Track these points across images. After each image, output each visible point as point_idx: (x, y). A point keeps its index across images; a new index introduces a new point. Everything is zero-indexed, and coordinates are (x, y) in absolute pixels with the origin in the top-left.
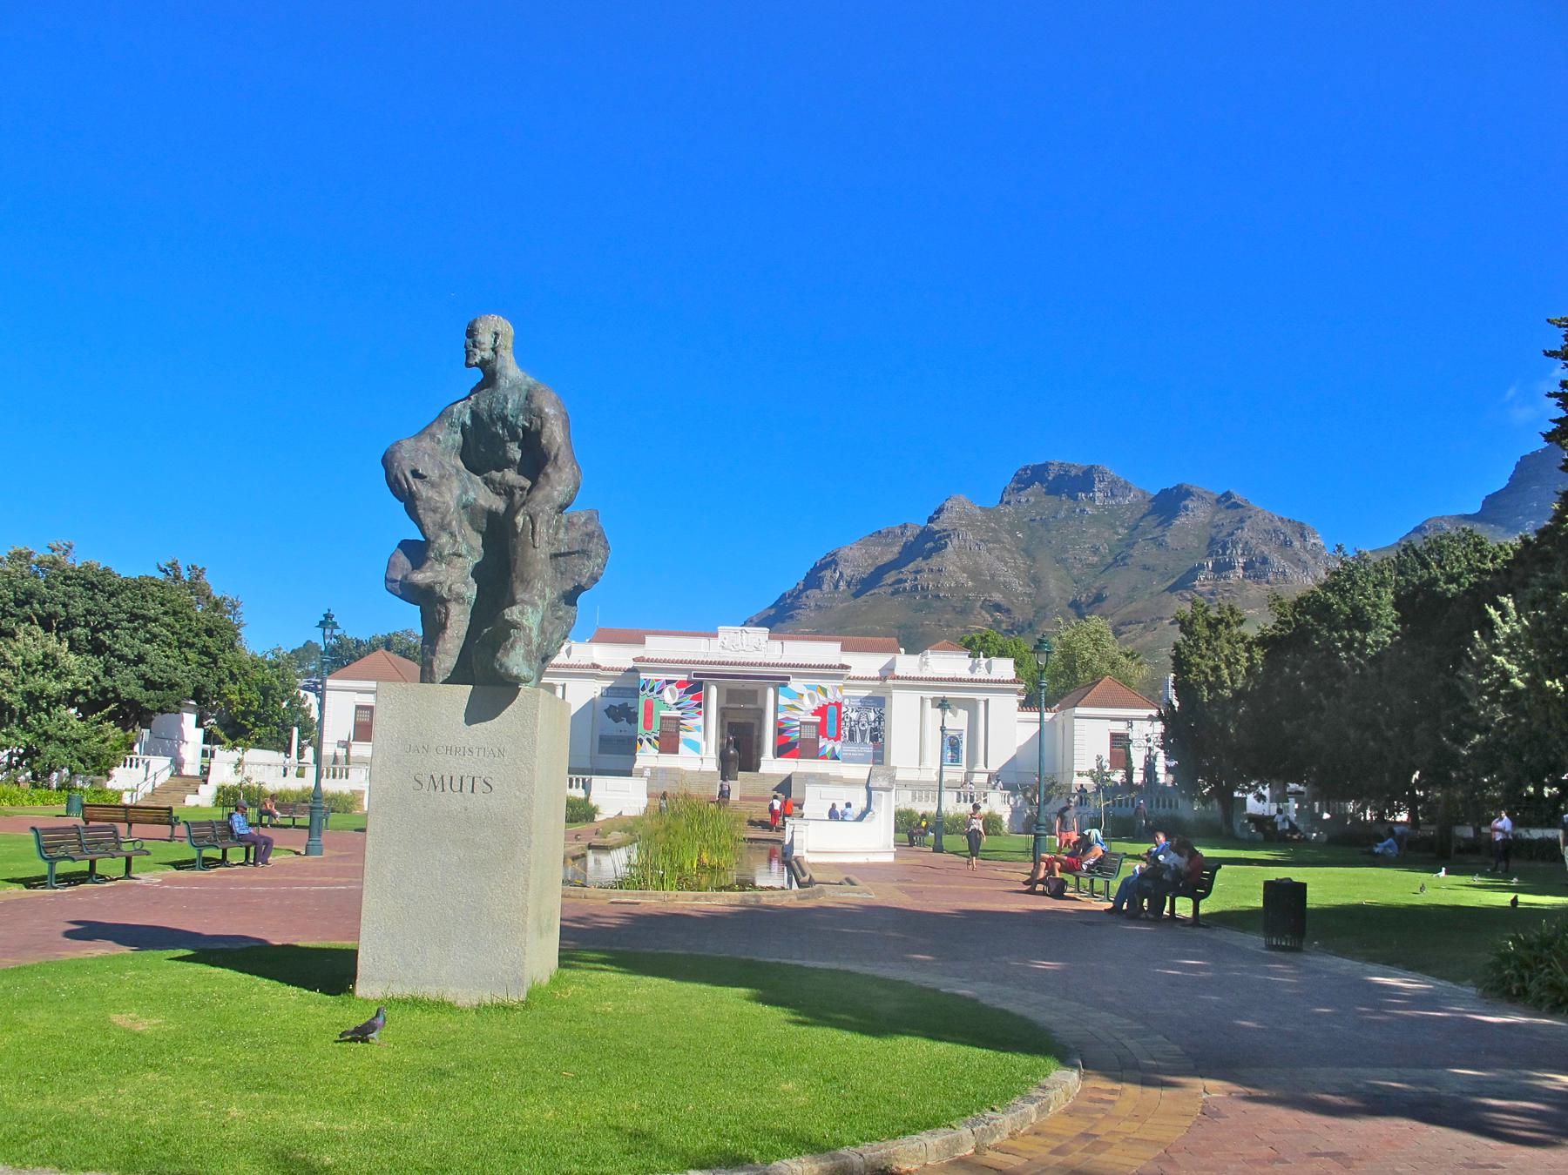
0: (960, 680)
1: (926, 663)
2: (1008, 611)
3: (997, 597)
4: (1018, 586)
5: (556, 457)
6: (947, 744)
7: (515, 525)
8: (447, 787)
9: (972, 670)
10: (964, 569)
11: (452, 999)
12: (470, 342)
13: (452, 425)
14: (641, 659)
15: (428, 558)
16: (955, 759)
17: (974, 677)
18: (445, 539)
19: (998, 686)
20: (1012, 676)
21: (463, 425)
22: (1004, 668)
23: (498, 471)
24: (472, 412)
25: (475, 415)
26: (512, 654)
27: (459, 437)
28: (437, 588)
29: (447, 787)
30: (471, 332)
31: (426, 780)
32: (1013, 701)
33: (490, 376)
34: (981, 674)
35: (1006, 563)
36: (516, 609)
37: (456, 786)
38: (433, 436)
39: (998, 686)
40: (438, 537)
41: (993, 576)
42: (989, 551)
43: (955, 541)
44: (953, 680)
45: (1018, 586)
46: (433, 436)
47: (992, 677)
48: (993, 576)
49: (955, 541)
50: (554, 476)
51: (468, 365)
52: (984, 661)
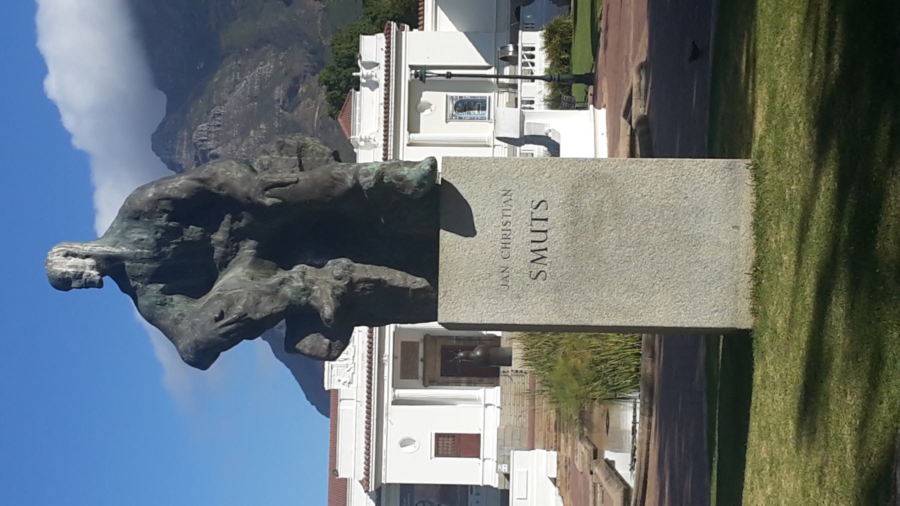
0: (387, 98)
1: (367, 140)
2: (296, 80)
3: (279, 93)
4: (267, 68)
5: (201, 181)
6: (464, 115)
7: (275, 205)
8: (542, 246)
9: (374, 85)
10: (244, 133)
11: (748, 277)
12: (75, 284)
13: (163, 304)
14: (365, 483)
15: (308, 304)
16: (481, 105)
17: (382, 82)
18: (287, 290)
19: (393, 53)
20: (381, 36)
21: (163, 291)
22: (372, 47)
23: (212, 250)
24: (150, 283)
25: (154, 278)
26: (409, 177)
27: (176, 298)
28: (338, 292)
29: (542, 246)
30: (63, 283)
31: (537, 268)
32: (410, 36)
33: (111, 266)
34: (379, 74)
35: (237, 82)
36: (362, 179)
37: (542, 236)
38: (176, 322)
39: (393, 53)
40: (285, 298)
41: (253, 98)
42: (222, 103)
43: (210, 144)
44: (387, 108)
45: (267, 68)
46: (176, 322)
47: (382, 61)
48: (253, 98)
49: (210, 144)
50: (221, 179)
51: (100, 285)
52: (364, 72)
